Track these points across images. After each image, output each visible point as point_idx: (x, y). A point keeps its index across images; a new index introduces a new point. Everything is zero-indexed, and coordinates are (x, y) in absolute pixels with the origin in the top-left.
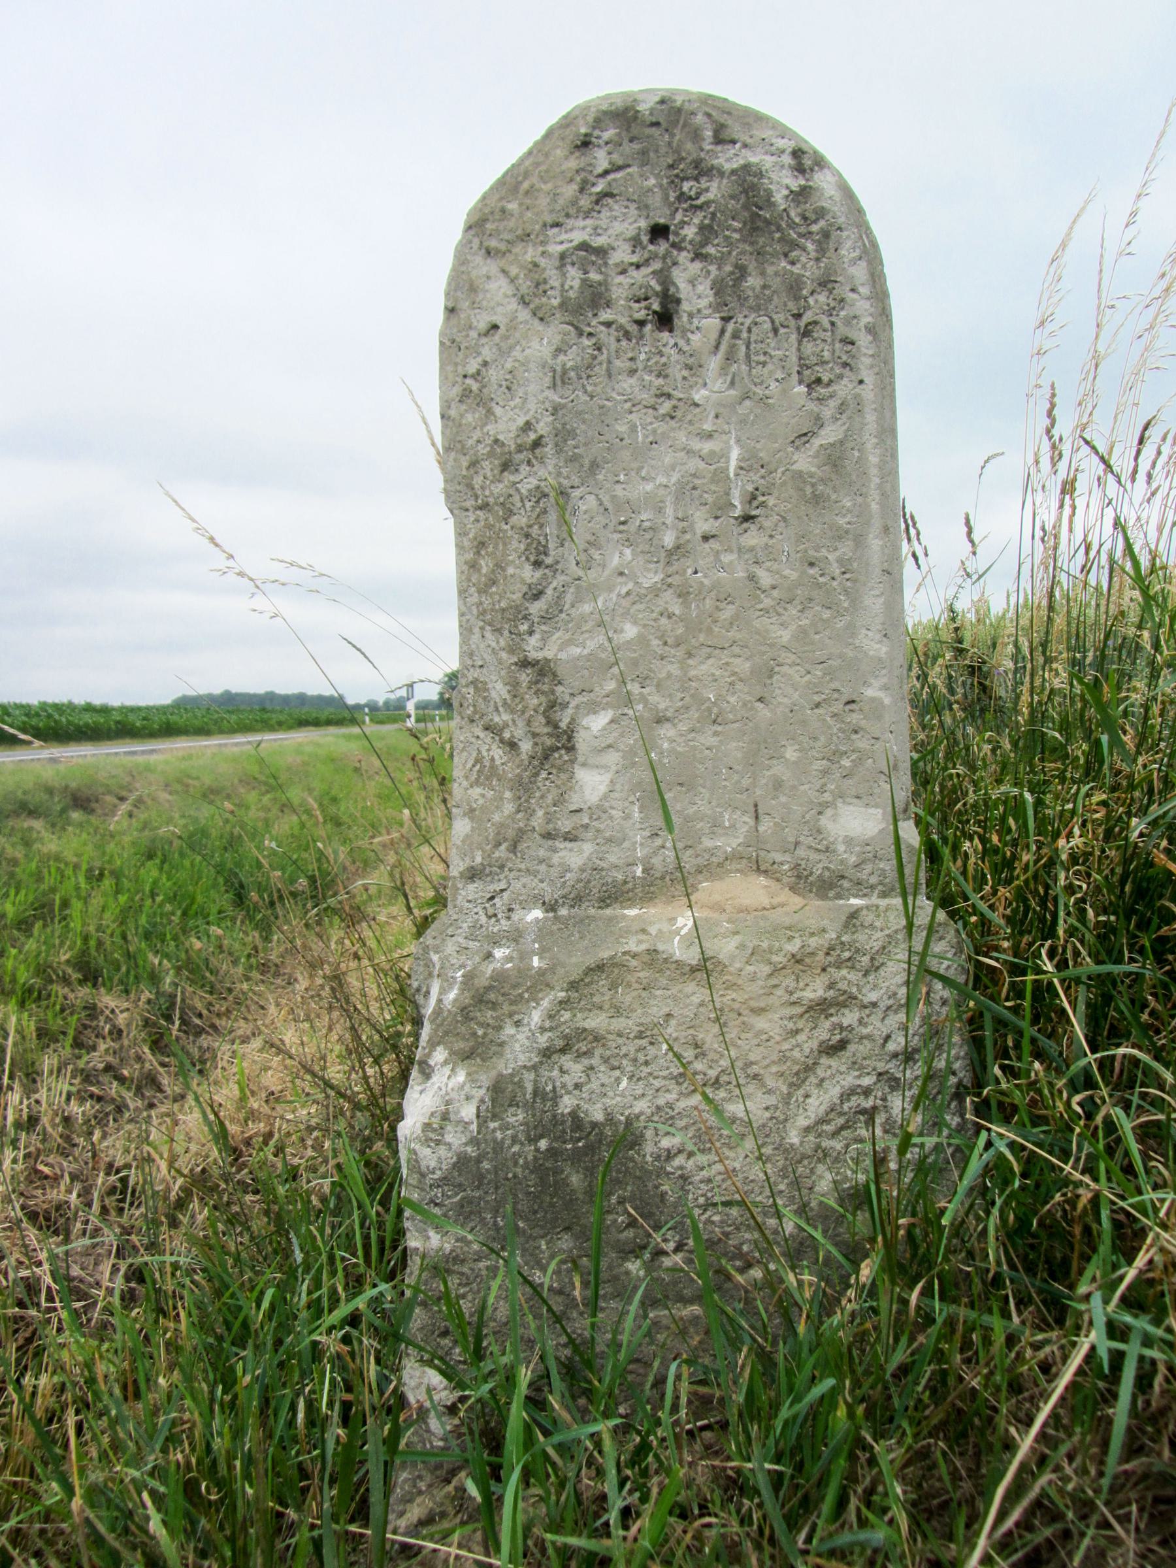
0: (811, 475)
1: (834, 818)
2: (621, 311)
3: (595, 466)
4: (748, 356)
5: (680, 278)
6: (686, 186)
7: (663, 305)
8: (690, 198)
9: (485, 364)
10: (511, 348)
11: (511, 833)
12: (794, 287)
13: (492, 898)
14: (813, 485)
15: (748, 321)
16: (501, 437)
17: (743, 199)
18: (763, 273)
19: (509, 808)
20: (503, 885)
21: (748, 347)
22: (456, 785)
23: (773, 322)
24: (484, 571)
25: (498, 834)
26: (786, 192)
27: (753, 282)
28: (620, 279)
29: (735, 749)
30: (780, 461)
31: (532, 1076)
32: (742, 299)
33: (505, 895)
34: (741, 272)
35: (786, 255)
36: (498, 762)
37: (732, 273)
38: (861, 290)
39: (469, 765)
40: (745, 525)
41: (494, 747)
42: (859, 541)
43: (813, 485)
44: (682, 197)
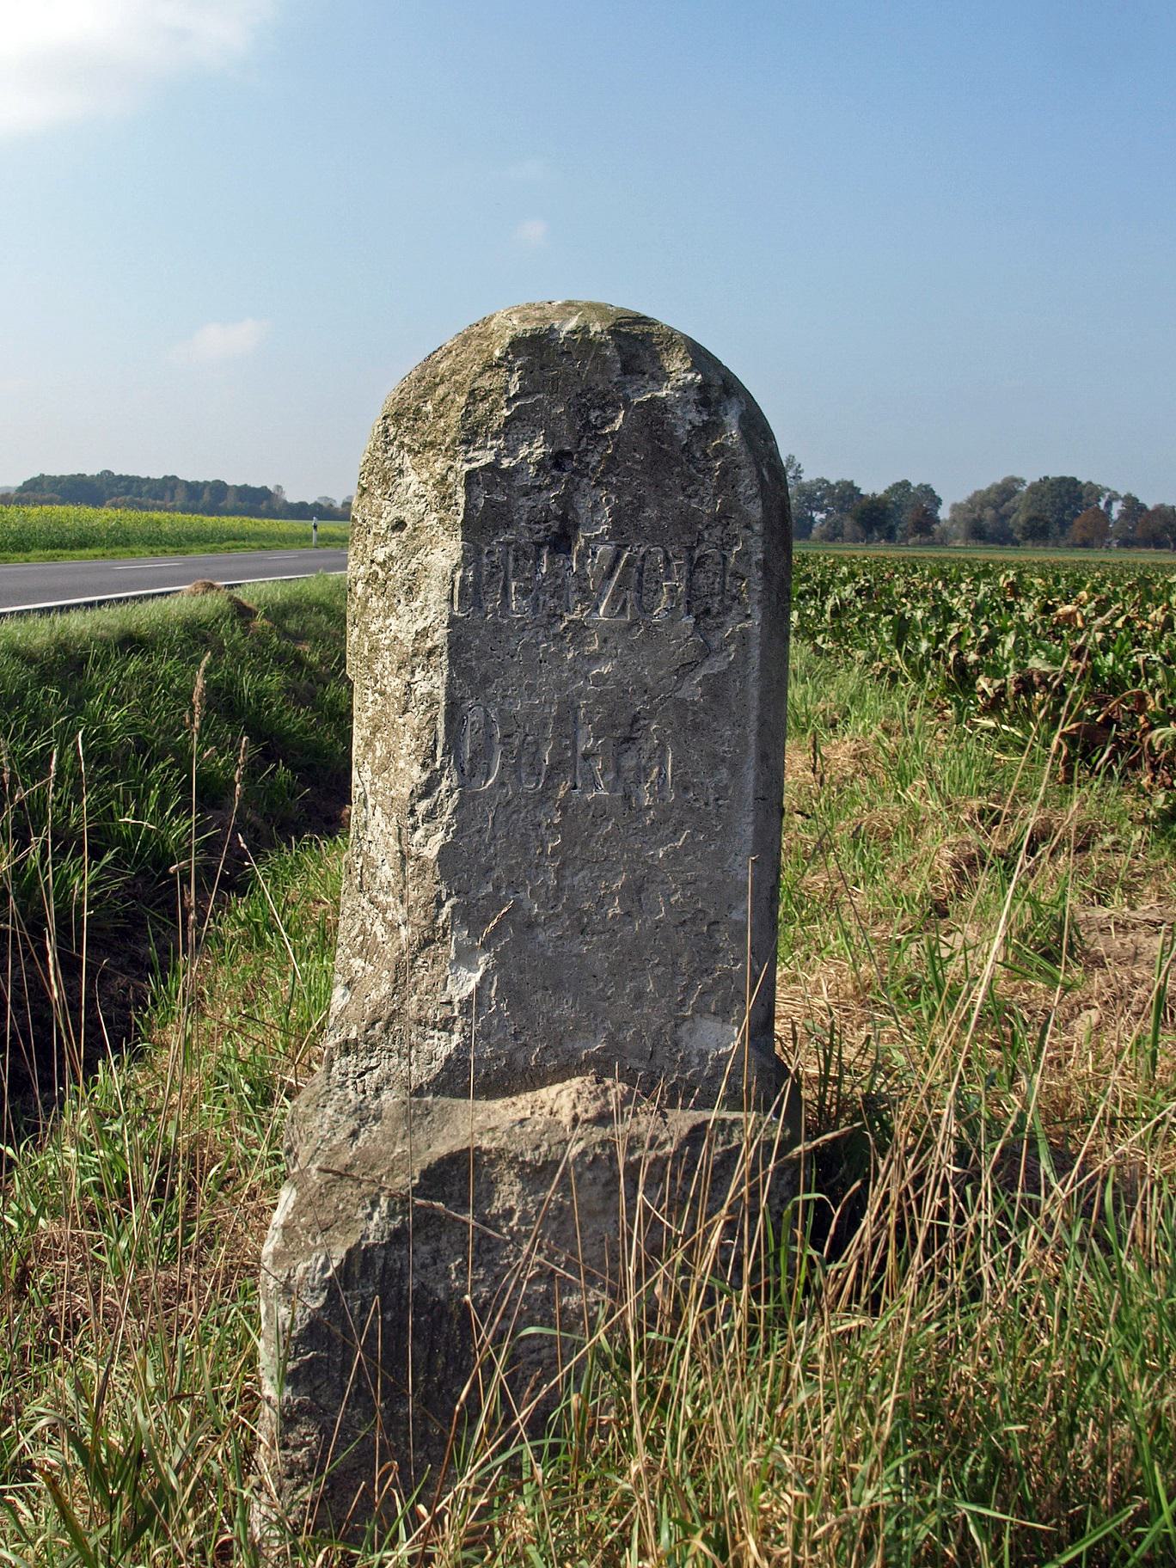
0: (694, 703)
1: (691, 1032)
2: (520, 533)
3: (486, 680)
4: (640, 582)
5: (584, 505)
6: (594, 415)
7: (562, 527)
8: (595, 427)
9: (391, 557)
10: (417, 550)
11: (385, 1013)
12: (688, 521)
13: (362, 1074)
14: (694, 713)
15: (642, 550)
16: (401, 636)
17: (647, 430)
18: (660, 505)
19: (386, 988)
20: (373, 1063)
21: (641, 575)
22: (339, 951)
23: (666, 552)
24: (378, 753)
25: (374, 1012)
26: (689, 427)
27: (651, 512)
28: (522, 501)
29: (600, 961)
30: (663, 689)
31: (383, 1254)
32: (639, 529)
33: (377, 1071)
34: (641, 504)
35: (684, 489)
36: (380, 939)
37: (631, 503)
38: (757, 527)
39: (353, 934)
40: (625, 746)
41: (377, 923)
42: (735, 770)
43: (694, 713)
44: (587, 425)
